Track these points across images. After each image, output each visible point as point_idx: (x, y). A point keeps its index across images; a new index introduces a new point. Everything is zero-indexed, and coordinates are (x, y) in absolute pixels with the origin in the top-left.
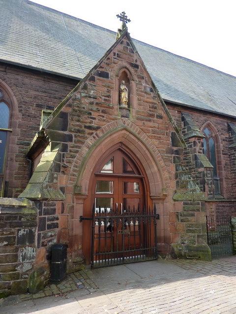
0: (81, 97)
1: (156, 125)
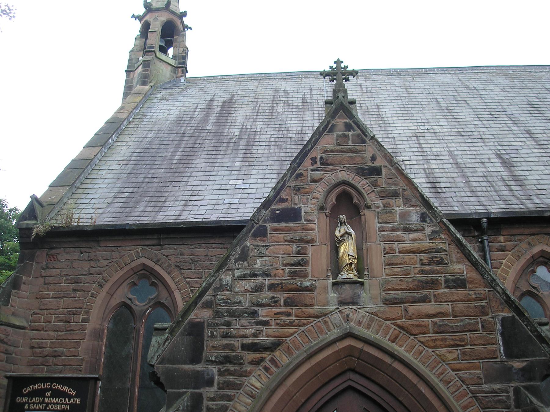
0: (234, 279)
1: (447, 307)
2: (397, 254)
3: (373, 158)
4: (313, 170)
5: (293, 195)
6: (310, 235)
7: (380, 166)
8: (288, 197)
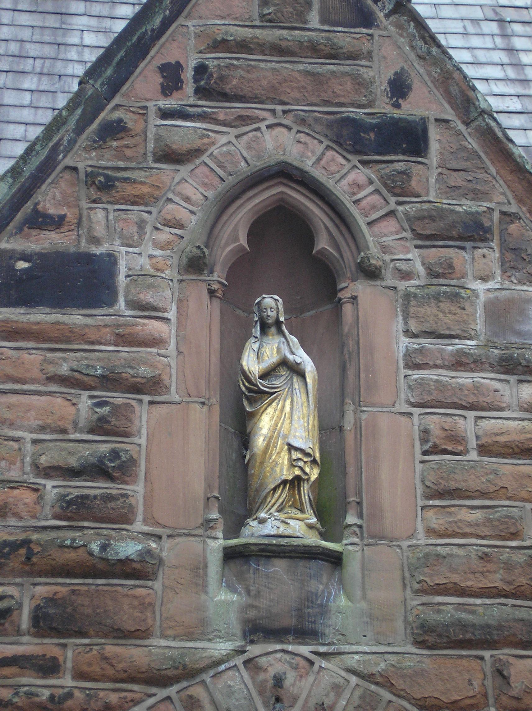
2: (473, 455)
3: (399, 88)
4: (165, 114)
5: (84, 204)
6: (143, 363)
7: (424, 121)
8: (64, 210)
